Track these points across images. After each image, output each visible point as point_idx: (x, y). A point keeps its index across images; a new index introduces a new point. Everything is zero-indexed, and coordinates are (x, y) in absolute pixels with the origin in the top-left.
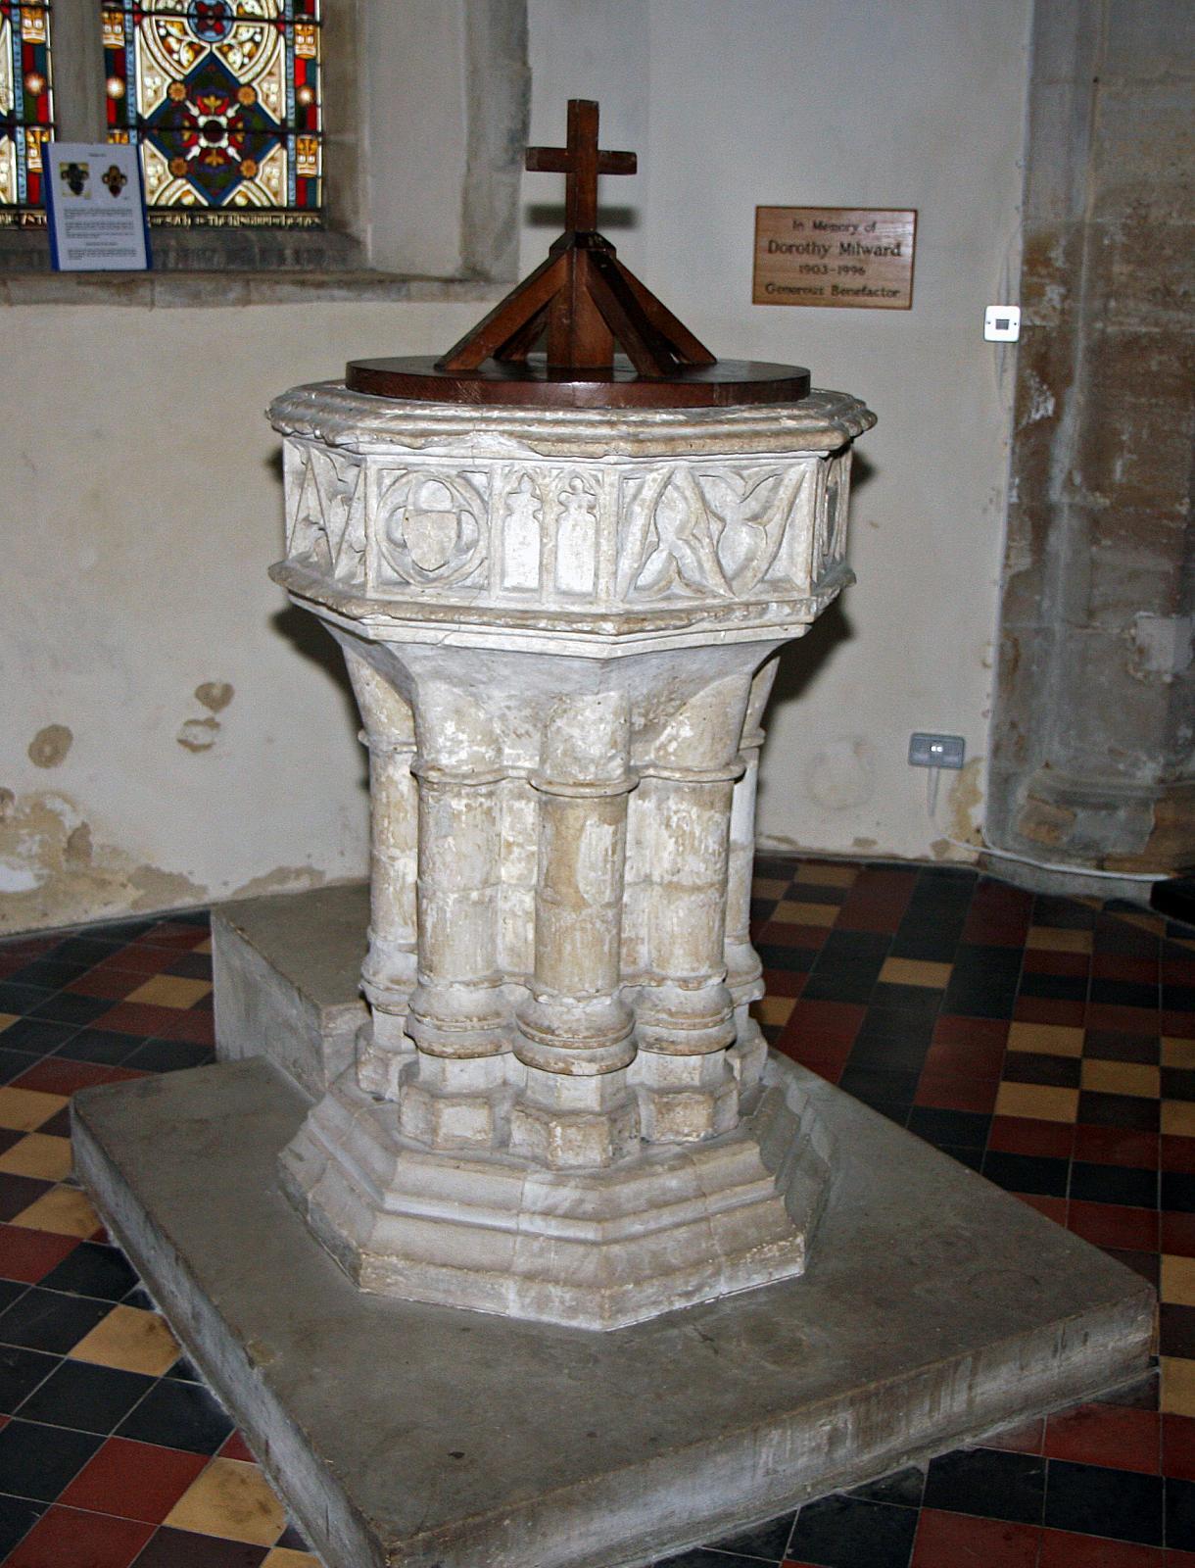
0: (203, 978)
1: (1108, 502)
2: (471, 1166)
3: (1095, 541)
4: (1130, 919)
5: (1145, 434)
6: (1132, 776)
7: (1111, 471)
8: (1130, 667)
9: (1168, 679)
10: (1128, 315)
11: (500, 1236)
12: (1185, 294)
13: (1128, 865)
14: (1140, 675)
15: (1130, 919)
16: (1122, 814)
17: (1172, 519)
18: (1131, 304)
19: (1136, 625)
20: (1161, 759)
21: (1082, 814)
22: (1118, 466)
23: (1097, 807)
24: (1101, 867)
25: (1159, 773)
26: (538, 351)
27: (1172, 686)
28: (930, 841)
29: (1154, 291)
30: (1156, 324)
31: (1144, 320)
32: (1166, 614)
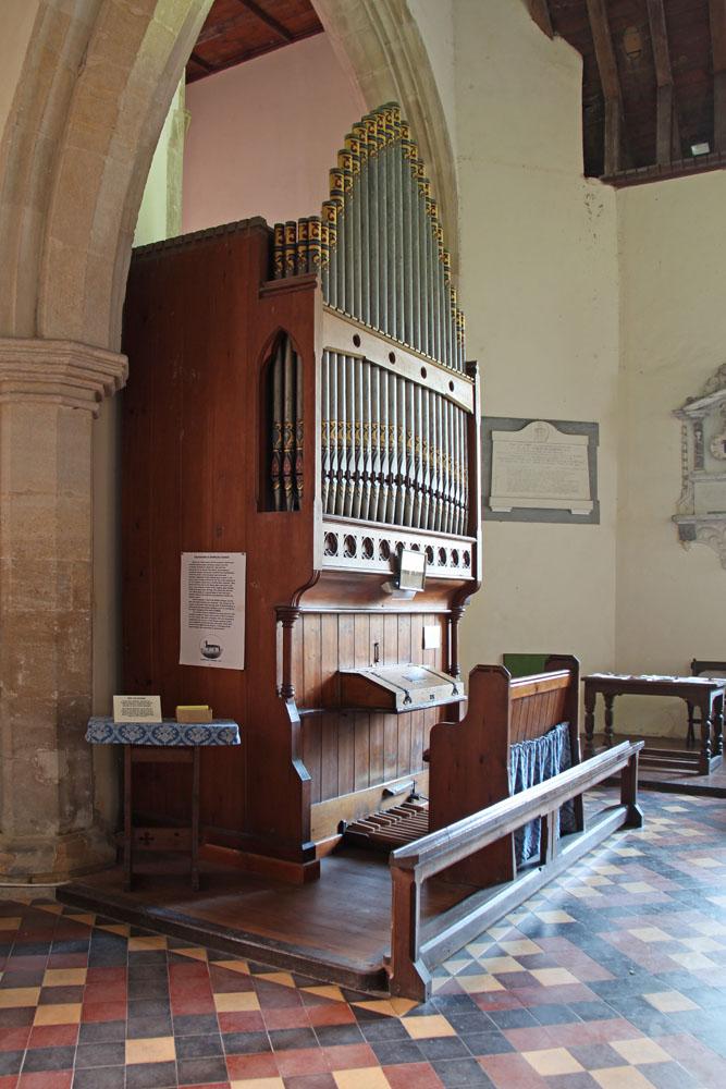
0: (487, 418)
1: (16, 695)
2: (283, 412)
3: (12, 715)
4: (44, 908)
5: (32, 661)
6: (44, 833)
7: (17, 679)
8: (37, 777)
9: (57, 782)
10: (18, 603)
11: (253, 414)
12: (46, 593)
13: (46, 879)
14: (42, 781)
15: (44, 908)
16: (39, 853)
17: (50, 702)
18: (19, 597)
19: (37, 756)
20: (58, 823)
21: (18, 856)
22: (20, 677)
23: (26, 851)
24: (30, 882)
25: (57, 830)
26: (538, 694)
27: (59, 785)
28: (284, 327)
29: (30, 592)
30: (32, 607)
31: (26, 606)
32: (51, 750)
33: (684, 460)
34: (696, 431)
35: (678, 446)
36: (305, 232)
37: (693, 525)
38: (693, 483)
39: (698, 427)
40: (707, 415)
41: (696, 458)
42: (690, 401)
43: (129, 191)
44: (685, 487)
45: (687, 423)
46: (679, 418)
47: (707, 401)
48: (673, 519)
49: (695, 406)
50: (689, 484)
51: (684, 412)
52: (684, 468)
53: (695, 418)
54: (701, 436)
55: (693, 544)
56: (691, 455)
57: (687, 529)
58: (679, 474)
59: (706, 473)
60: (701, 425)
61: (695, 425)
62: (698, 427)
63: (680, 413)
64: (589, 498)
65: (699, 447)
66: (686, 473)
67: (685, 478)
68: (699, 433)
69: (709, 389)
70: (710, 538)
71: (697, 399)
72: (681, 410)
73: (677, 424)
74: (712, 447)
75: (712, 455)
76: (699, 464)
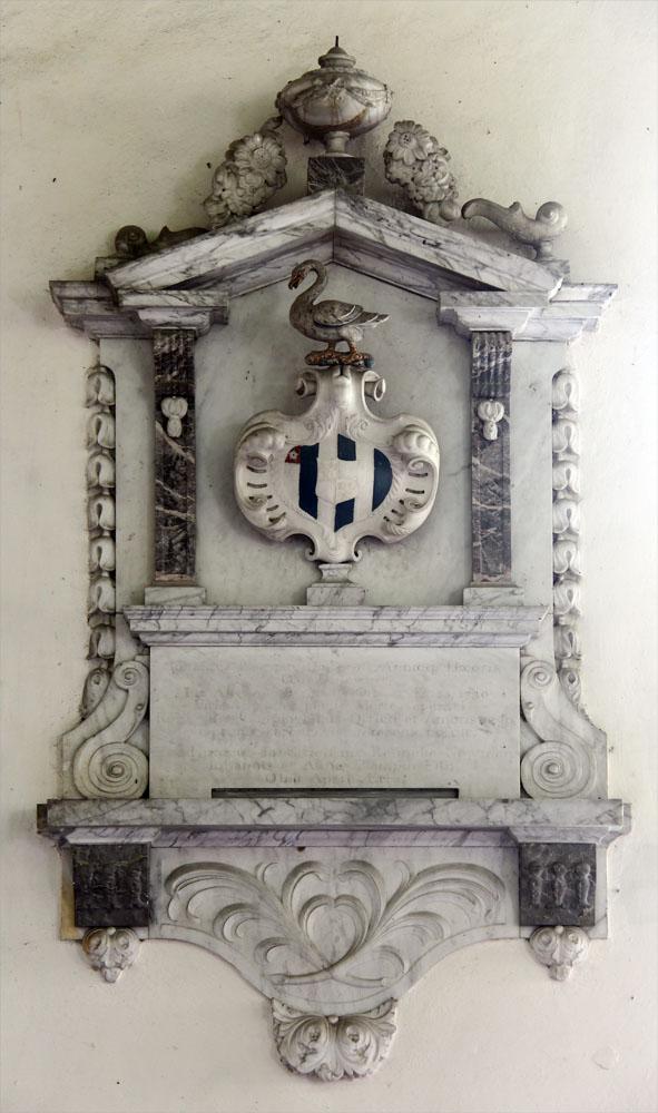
0: (602, 939)
33: (97, 532)
34: (161, 394)
35: (70, 467)
36: (492, 412)
37: (140, 855)
38: (145, 649)
39: (173, 373)
40: (220, 318)
41: (160, 523)
42: (134, 245)
43: (473, 550)
44: (105, 666)
45: (112, 353)
46: (77, 325)
47: (224, 250)
48: (47, 820)
49: (164, 268)
50: (125, 650)
51: (112, 297)
52: (96, 573)
53: (166, 331)
54: (187, 421)
55: (140, 949)
56: (133, 513)
57: (117, 865)
58: (70, 598)
59: (213, 605)
60: (189, 370)
61: (163, 362)
62: (173, 373)
63: (94, 297)
64: (146, 929)
65: (173, 474)
66: (107, 596)
67: (104, 621)
68: (175, 408)
69: (234, 194)
70: (224, 913)
71: (170, 239)
72: (100, 280)
73: (69, 357)
74: (242, 476)
75: (237, 515)
76: (174, 554)
